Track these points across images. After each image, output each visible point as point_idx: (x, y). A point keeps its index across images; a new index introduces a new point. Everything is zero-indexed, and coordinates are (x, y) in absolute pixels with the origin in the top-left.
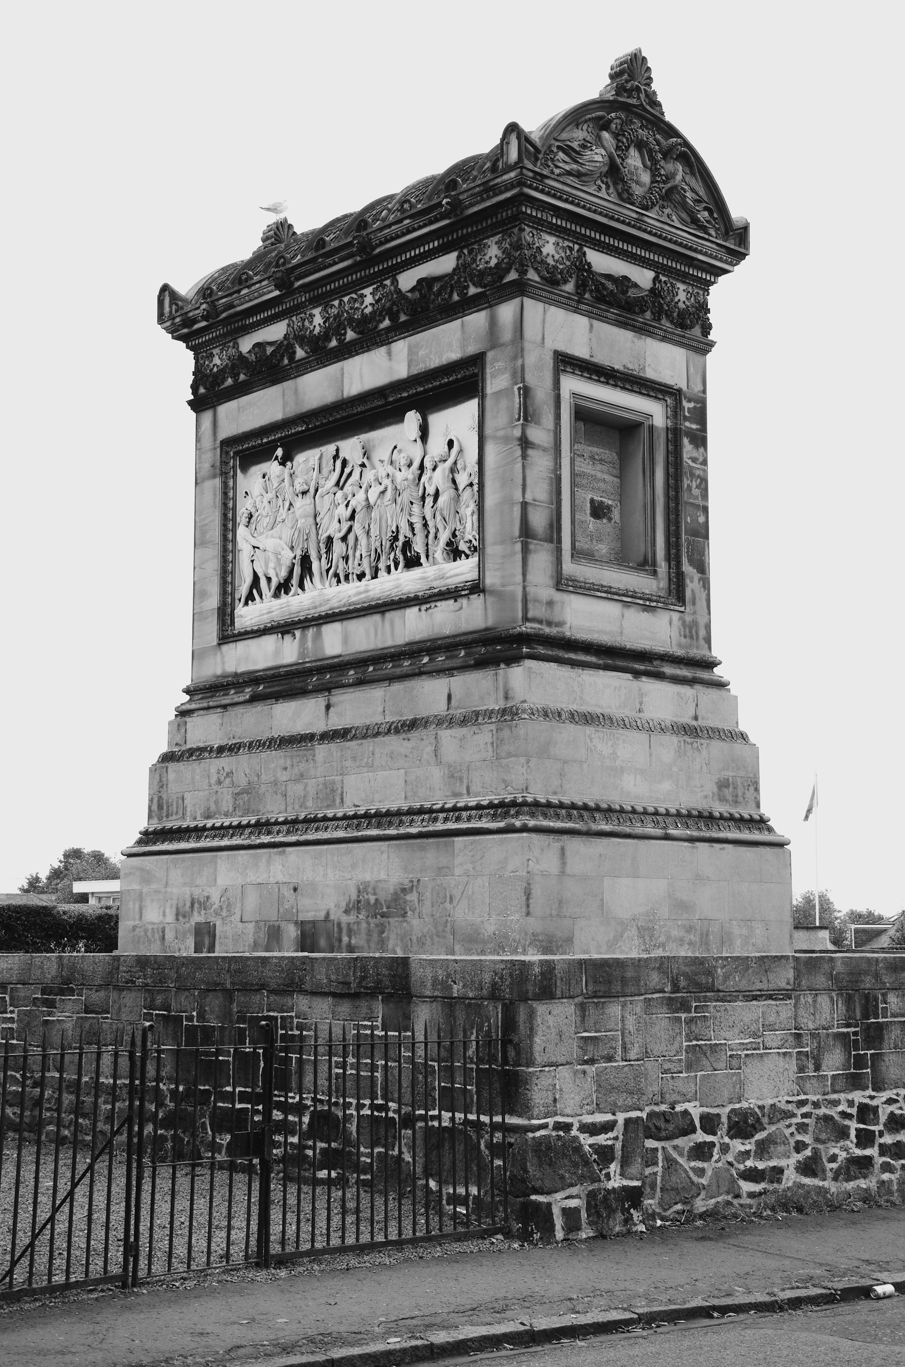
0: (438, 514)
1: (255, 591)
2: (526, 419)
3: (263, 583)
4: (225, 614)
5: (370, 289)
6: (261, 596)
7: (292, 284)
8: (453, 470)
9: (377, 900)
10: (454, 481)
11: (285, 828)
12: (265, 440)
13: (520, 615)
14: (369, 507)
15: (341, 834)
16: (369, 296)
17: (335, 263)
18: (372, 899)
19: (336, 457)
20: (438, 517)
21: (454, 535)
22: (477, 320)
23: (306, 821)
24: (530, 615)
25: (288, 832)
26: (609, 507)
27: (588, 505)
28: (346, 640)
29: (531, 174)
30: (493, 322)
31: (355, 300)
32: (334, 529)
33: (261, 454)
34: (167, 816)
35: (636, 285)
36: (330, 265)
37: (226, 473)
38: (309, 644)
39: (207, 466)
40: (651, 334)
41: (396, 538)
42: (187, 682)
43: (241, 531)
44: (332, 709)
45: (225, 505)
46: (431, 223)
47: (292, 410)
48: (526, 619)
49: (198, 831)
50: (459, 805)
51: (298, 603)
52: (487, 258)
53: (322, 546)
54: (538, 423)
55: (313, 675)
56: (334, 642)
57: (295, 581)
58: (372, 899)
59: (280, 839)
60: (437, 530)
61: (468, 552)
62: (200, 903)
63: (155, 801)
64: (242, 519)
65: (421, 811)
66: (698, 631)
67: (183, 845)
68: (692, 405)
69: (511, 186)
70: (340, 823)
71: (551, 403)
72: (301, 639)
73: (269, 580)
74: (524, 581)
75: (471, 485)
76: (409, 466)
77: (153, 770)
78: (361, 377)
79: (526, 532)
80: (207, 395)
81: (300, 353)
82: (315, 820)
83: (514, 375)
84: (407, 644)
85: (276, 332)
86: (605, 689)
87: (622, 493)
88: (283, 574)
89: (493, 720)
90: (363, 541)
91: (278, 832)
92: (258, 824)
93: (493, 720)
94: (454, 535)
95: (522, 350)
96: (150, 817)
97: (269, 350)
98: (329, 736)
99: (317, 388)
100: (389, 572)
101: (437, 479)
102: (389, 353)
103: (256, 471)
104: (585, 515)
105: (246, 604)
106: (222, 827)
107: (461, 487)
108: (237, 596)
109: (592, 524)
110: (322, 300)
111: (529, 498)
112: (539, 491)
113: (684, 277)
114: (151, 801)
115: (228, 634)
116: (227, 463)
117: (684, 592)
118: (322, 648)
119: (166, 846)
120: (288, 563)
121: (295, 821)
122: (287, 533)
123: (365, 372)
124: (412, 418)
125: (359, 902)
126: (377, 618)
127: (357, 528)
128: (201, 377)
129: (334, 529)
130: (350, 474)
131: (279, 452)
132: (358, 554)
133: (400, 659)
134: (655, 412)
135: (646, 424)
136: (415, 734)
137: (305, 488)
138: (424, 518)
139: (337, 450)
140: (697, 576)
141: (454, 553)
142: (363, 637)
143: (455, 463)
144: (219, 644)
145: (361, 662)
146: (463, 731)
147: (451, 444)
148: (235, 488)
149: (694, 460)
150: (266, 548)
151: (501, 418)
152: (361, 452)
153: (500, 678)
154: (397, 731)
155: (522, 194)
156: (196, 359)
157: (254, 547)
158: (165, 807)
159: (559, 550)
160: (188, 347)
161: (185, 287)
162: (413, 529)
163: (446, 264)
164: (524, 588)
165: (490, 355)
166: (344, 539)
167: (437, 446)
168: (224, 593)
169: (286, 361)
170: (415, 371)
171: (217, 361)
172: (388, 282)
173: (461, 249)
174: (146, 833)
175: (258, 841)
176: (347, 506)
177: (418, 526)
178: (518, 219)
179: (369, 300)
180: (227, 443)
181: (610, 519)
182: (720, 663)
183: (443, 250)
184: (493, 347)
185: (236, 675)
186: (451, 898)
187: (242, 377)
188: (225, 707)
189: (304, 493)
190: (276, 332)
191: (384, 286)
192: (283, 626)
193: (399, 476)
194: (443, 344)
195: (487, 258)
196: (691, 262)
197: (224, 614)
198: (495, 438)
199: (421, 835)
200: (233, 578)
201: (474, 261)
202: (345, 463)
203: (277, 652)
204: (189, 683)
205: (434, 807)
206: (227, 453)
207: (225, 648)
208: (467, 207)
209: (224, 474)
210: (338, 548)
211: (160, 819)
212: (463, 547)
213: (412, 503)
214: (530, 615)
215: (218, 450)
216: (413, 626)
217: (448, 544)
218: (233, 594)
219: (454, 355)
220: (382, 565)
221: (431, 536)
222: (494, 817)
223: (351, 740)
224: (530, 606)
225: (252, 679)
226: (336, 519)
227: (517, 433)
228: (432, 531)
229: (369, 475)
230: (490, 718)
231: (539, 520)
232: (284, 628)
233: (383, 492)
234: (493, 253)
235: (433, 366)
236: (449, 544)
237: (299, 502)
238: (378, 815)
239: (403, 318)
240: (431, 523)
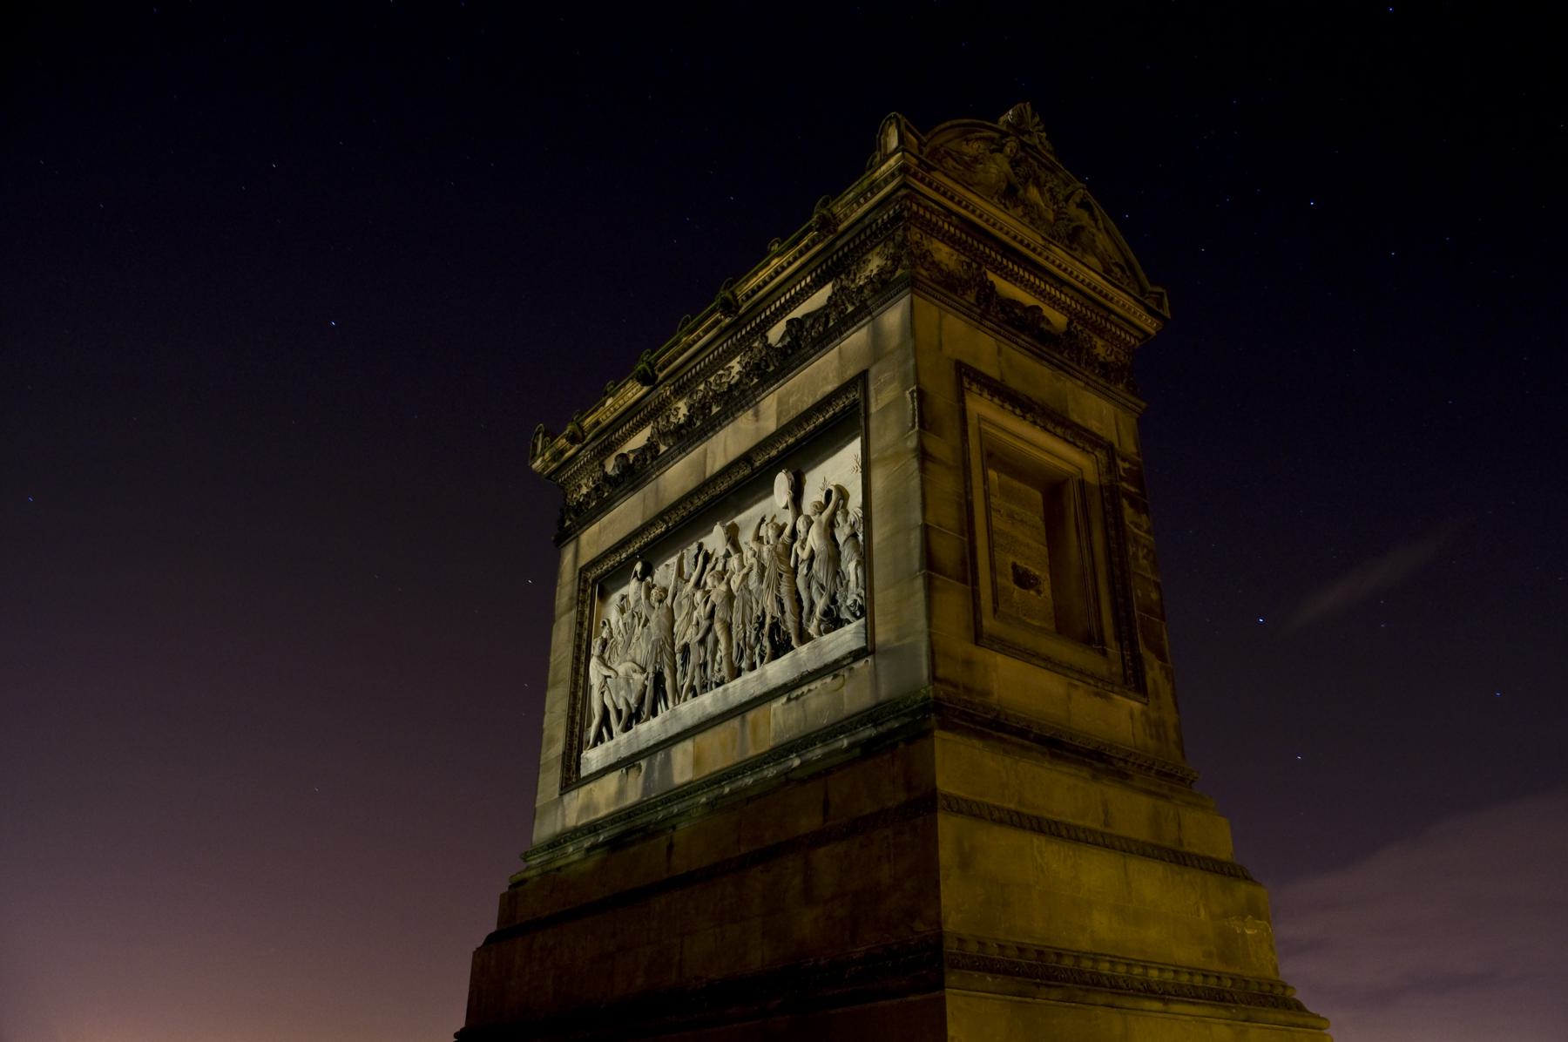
8: (831, 524)
17: (700, 338)
20: (814, 587)
22: (857, 339)
24: (940, 672)
26: (1036, 578)
27: (1010, 570)
30: (877, 336)
33: (619, 575)
48: (934, 678)
53: (678, 657)
57: (646, 708)
68: (1127, 465)
73: (619, 712)
79: (930, 562)
85: (639, 440)
86: (1060, 790)
99: (677, 478)
104: (1007, 582)
109: (1017, 592)
111: (931, 521)
116: (585, 591)
117: (1144, 678)
120: (639, 687)
123: (726, 445)
124: (782, 482)
131: (638, 567)
141: (833, 621)
159: (975, 596)
164: (930, 635)
165: (873, 371)
166: (702, 642)
167: (813, 494)
170: (784, 421)
173: (837, 276)
179: (737, 368)
183: (817, 285)
184: (875, 362)
190: (639, 440)
197: (570, 757)
207: (567, 798)
212: (846, 615)
232: (627, 763)
235: (805, 407)
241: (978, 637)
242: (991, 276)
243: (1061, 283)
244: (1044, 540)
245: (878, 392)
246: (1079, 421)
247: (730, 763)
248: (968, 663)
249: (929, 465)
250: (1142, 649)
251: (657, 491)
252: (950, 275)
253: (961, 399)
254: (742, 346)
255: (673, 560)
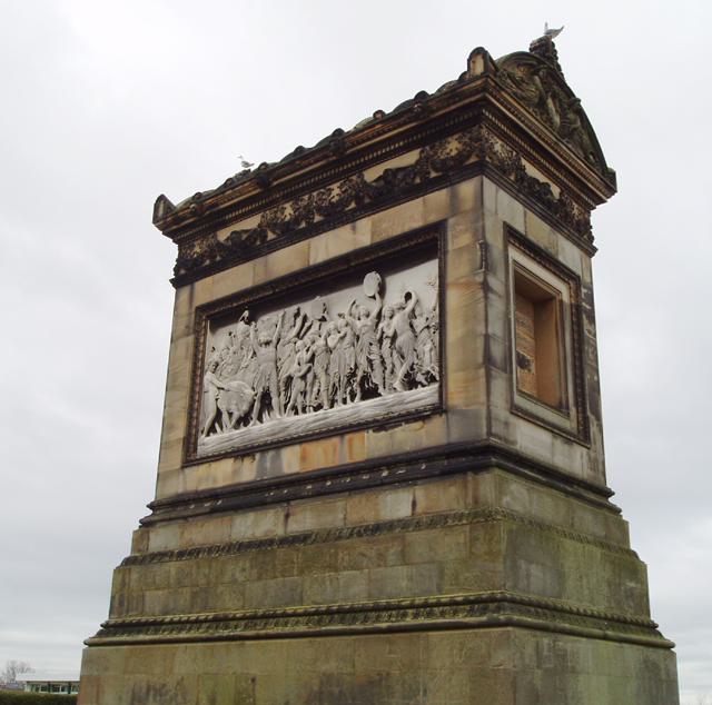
0: (395, 352)
1: (217, 425)
2: (486, 268)
3: (225, 417)
4: (190, 443)
5: (338, 184)
6: (222, 428)
7: (270, 183)
9: (340, 692)
10: (411, 326)
11: (243, 623)
12: (235, 305)
13: (485, 430)
14: (329, 351)
15: (302, 628)
16: (336, 190)
18: (336, 690)
19: (297, 315)
21: (412, 369)
22: (439, 197)
23: (264, 617)
25: (246, 627)
26: (528, 361)
28: (304, 458)
29: (493, 84)
30: (454, 197)
31: (324, 194)
32: (292, 368)
34: (128, 611)
35: (552, 194)
36: (306, 166)
37: (199, 332)
38: (268, 464)
39: (182, 327)
40: (561, 232)
41: (353, 374)
42: (152, 499)
43: (208, 376)
44: (291, 518)
45: (196, 355)
46: (400, 126)
47: (261, 279)
48: (490, 433)
49: (156, 625)
50: (430, 601)
51: (258, 430)
52: (448, 151)
54: (495, 274)
55: (271, 490)
56: (291, 462)
57: (254, 414)
58: (336, 690)
59: (238, 632)
60: (394, 366)
61: (425, 383)
62: (155, 690)
63: (117, 597)
64: (209, 366)
65: (388, 608)
66: (598, 464)
67: (141, 637)
69: (477, 91)
70: (300, 619)
71: (502, 261)
72: (260, 460)
73: (230, 414)
74: (488, 400)
75: (428, 327)
76: (368, 316)
77: (117, 571)
78: (327, 248)
79: (488, 360)
80: (185, 276)
81: (271, 236)
82: (274, 616)
83: (475, 234)
84: (366, 461)
85: (252, 223)
87: (539, 351)
88: (245, 407)
89: (464, 522)
90: (323, 378)
91: (236, 627)
92: (216, 620)
93: (464, 522)
94: (412, 369)
95: (483, 214)
96: (111, 612)
97: (244, 236)
98: (284, 541)
99: (285, 261)
100: (345, 401)
101: (396, 323)
102: (354, 229)
103: (223, 332)
105: (208, 435)
106: (180, 622)
107: (418, 330)
108: (201, 429)
110: (293, 196)
112: (496, 328)
113: (578, 199)
114: (113, 598)
115: (191, 458)
118: (280, 467)
119: (125, 638)
120: (250, 399)
121: (254, 617)
122: (250, 376)
124: (372, 279)
125: (321, 693)
126: (336, 440)
127: (318, 368)
128: (181, 262)
129: (292, 368)
130: (310, 327)
131: (246, 314)
132: (315, 389)
133: (359, 474)
134: (563, 290)
135: (558, 298)
136: (381, 536)
137: (269, 339)
138: (381, 357)
139: (299, 309)
140: (595, 423)
141: (411, 383)
142: (322, 456)
143: (413, 310)
144: (183, 467)
145: (319, 477)
146: (433, 533)
147: (408, 296)
148: (204, 343)
149: (590, 332)
150: (228, 387)
151: (459, 268)
152: (322, 308)
153: (470, 486)
154: (360, 535)
155: (485, 99)
156: (180, 249)
157: (219, 388)
158: (126, 604)
160: (174, 241)
161: (177, 200)
162: (372, 366)
163: (410, 158)
164: (488, 407)
165: (451, 221)
166: (304, 377)
167: (394, 297)
168: (189, 426)
169: (258, 243)
170: (378, 240)
171: (197, 249)
172: (354, 178)
174: (106, 626)
175: (217, 635)
176: (308, 350)
177: (377, 363)
178: (478, 120)
180: (202, 309)
181: (529, 371)
182: (613, 494)
184: (453, 216)
185: (197, 492)
186: (425, 691)
187: (218, 258)
188: (185, 518)
189: (267, 343)
190: (252, 223)
191: (351, 181)
192: (243, 450)
193: (359, 324)
194: (407, 217)
195: (448, 151)
196: (583, 187)
197: (189, 443)
198: (456, 284)
199: (390, 630)
200: (199, 414)
201: (436, 154)
202: (305, 319)
203: (236, 472)
204: (153, 500)
205: (403, 603)
206: (201, 317)
207: (187, 471)
208: (433, 112)
209: (197, 332)
210: (298, 385)
211: (120, 615)
212: (420, 378)
213: (371, 344)
214: (493, 430)
215: (193, 316)
216: (371, 445)
217: (406, 376)
218: (197, 426)
219: (417, 224)
220: (339, 397)
221: (388, 372)
222: (471, 612)
223: (312, 543)
224: (493, 423)
225: (213, 495)
226: (296, 361)
227: (480, 279)
228: (389, 367)
229: (329, 326)
230: (460, 520)
231: (497, 351)
232: (242, 453)
233: (342, 338)
234: (453, 146)
235: (395, 234)
236: (407, 375)
237: (263, 350)
238: (341, 611)
239: (367, 201)
240: (388, 361)
241: (516, 410)
242: (524, 162)
243: (559, 166)
244: (532, 335)
245: (455, 237)
246: (564, 262)
247: (331, 465)
248: (506, 424)
249: (490, 295)
250: (589, 413)
251: (266, 265)
252: (502, 161)
253: (506, 250)
254: (343, 176)
255: (281, 313)
